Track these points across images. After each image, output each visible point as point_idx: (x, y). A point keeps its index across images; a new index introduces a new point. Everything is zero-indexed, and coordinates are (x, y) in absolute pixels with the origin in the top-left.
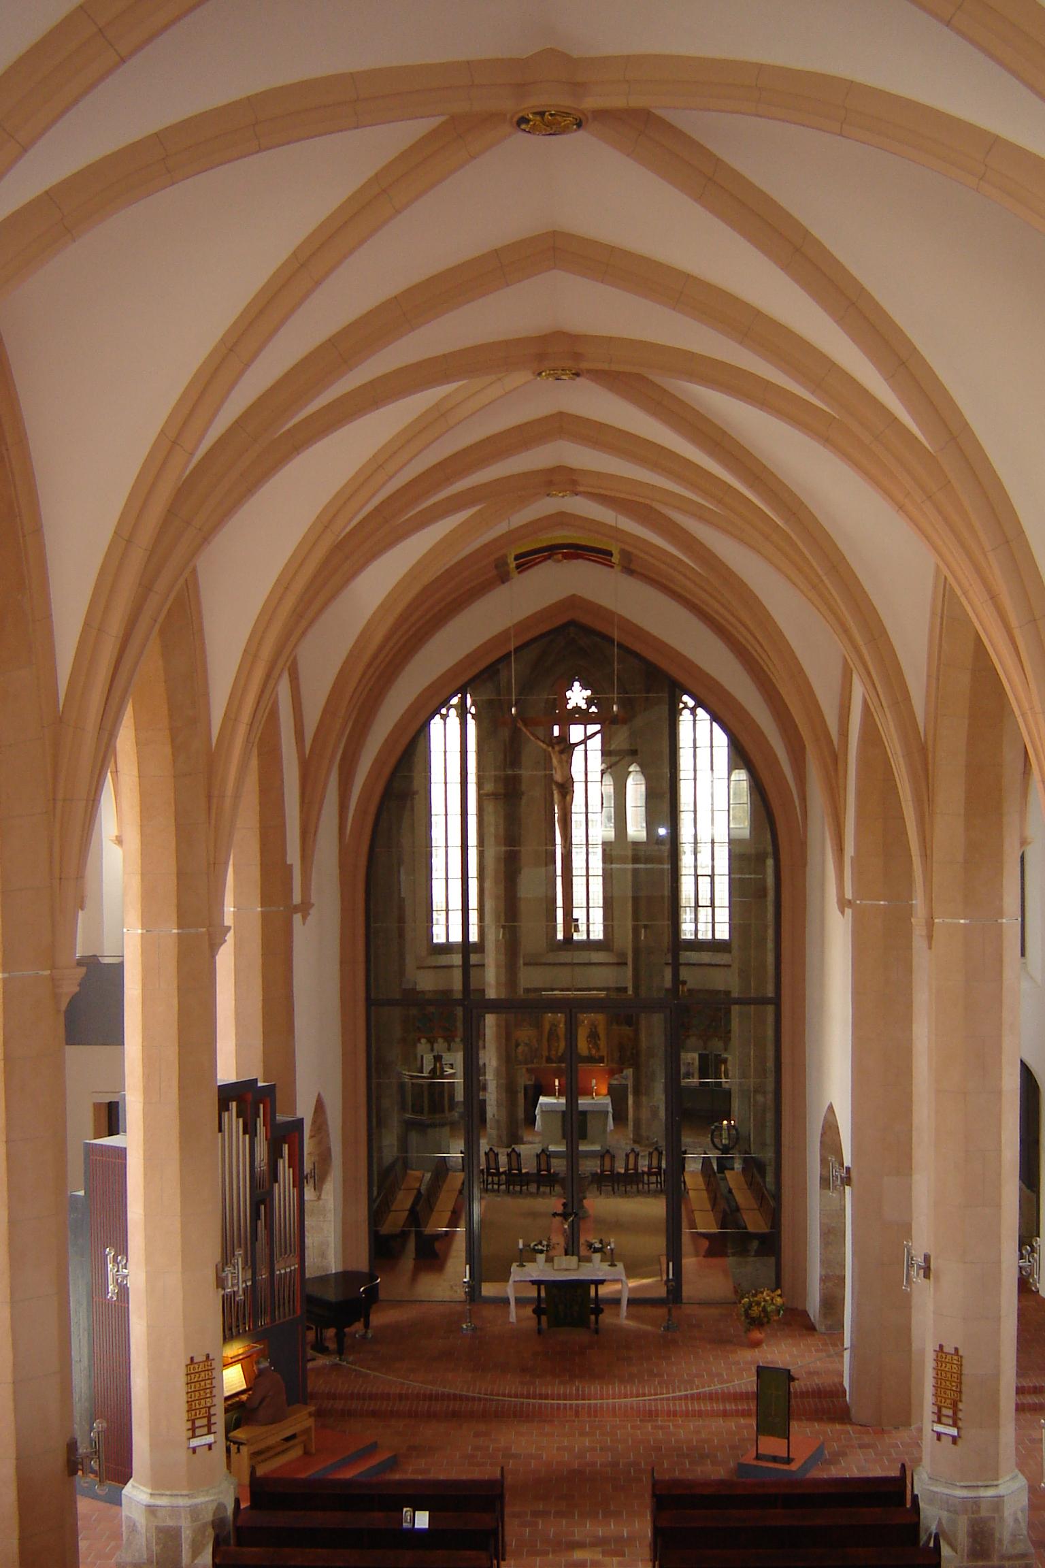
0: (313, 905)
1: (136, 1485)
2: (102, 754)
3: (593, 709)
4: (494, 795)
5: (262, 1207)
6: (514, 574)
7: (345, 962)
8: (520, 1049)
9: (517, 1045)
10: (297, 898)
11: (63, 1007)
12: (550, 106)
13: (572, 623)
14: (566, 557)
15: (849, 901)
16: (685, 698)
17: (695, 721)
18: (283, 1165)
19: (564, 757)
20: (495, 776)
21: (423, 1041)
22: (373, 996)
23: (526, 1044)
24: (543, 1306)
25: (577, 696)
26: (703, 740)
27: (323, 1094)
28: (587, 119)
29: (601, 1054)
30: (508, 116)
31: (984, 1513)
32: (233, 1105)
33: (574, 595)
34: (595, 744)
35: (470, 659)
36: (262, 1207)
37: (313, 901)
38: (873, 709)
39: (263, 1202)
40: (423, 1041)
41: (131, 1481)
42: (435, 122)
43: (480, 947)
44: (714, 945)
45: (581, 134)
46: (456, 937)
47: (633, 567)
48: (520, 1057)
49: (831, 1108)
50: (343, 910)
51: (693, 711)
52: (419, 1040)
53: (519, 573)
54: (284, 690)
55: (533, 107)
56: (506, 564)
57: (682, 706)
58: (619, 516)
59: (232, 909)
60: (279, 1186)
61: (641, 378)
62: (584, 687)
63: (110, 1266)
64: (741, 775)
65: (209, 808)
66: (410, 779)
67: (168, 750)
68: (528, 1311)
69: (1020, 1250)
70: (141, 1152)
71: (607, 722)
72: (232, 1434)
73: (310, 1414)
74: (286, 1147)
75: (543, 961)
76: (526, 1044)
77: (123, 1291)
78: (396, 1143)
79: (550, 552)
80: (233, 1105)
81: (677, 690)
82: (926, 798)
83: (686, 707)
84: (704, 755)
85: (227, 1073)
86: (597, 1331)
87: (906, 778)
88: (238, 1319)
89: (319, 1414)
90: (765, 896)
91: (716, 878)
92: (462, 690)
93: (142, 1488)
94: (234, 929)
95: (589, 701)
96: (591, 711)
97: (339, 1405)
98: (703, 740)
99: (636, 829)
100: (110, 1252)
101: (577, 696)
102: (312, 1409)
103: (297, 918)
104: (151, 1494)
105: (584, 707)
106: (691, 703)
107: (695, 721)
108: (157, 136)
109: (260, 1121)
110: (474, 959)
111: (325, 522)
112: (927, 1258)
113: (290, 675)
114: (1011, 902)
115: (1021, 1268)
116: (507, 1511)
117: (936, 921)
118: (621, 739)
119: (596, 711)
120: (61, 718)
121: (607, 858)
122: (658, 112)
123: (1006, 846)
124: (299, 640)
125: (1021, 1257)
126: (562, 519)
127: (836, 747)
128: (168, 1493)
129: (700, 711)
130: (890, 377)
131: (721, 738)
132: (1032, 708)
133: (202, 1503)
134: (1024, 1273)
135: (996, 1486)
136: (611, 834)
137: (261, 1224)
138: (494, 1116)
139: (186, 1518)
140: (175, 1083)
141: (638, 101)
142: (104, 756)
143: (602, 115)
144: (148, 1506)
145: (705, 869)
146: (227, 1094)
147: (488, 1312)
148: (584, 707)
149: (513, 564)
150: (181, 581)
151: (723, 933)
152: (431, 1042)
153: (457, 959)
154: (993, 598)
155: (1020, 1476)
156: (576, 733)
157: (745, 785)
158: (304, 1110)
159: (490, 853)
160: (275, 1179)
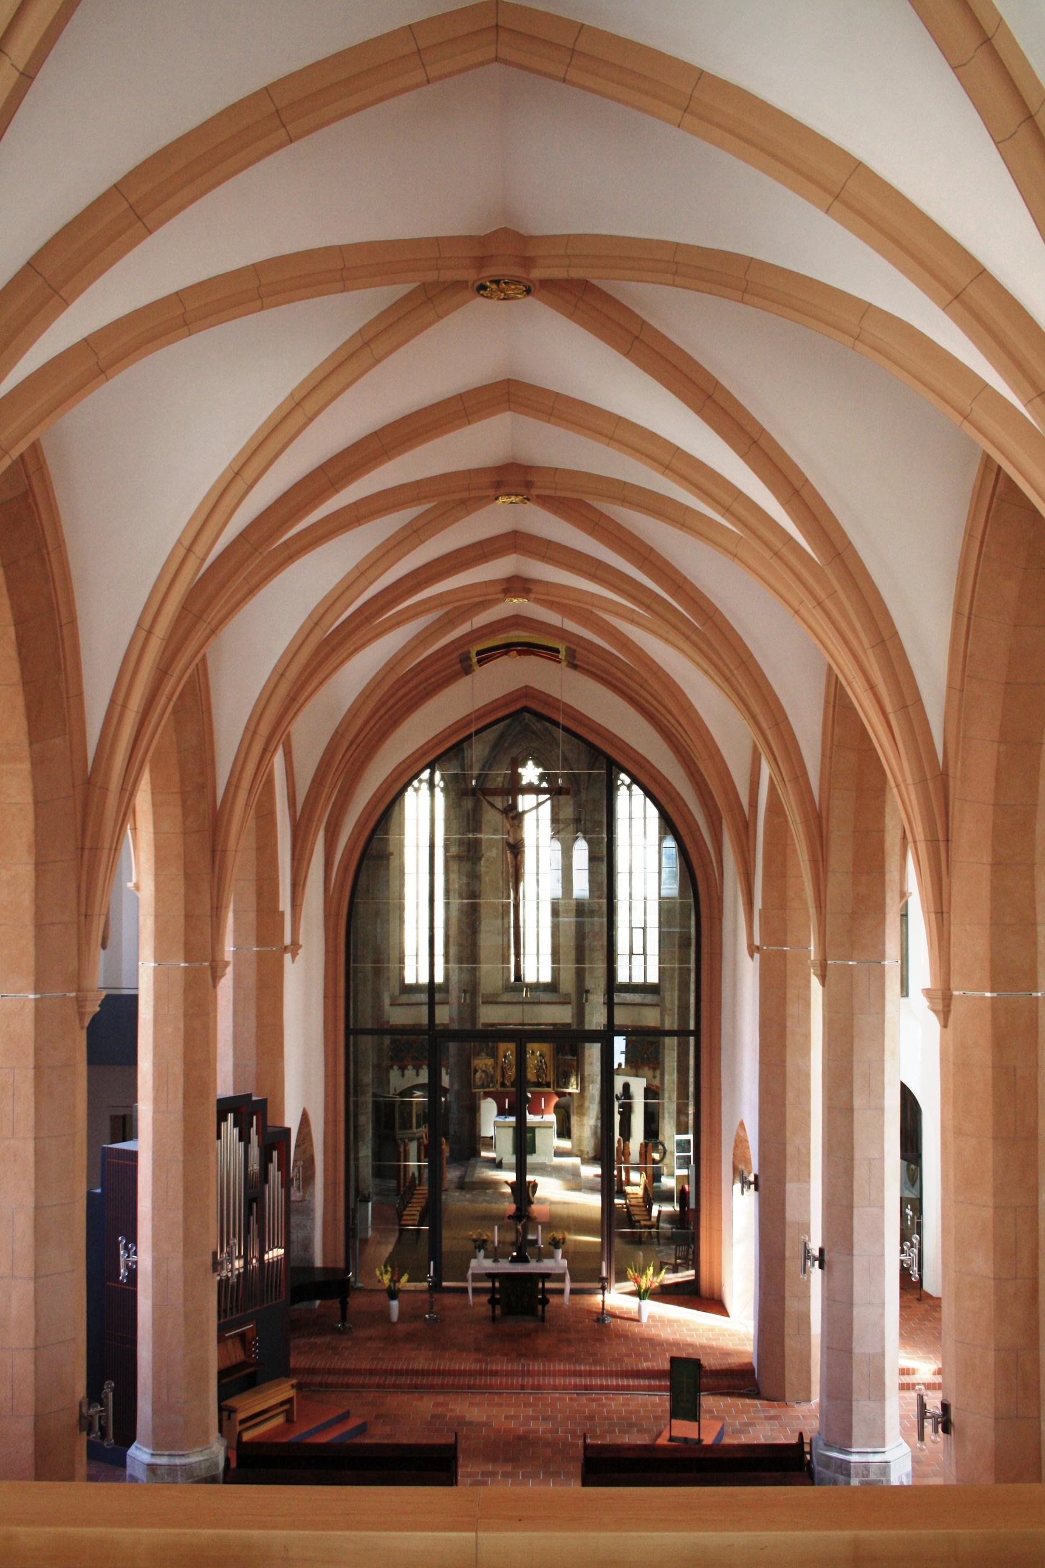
0: (301, 946)
1: (139, 1446)
2: (123, 810)
3: (544, 785)
4: (459, 858)
5: (255, 1205)
6: (476, 667)
7: (328, 996)
8: (478, 1075)
9: (476, 1071)
10: (287, 940)
11: (87, 1024)
12: (504, 275)
13: (525, 709)
14: (520, 653)
15: (758, 948)
16: (623, 776)
17: (631, 795)
18: (273, 1167)
19: (516, 822)
20: (460, 839)
21: (396, 1068)
22: (351, 1027)
23: (483, 1071)
24: (498, 1296)
25: (530, 773)
26: (638, 812)
27: (308, 1110)
28: (535, 288)
29: (548, 1080)
30: (470, 284)
31: (873, 1477)
32: (230, 1117)
33: (526, 686)
34: (546, 810)
35: (439, 739)
36: (255, 1205)
37: (301, 942)
38: (776, 783)
39: (255, 1200)
40: (396, 1068)
41: (135, 1443)
42: (412, 286)
43: (445, 987)
44: (644, 988)
45: (530, 299)
46: (424, 979)
47: (576, 662)
48: (479, 1083)
49: (742, 1124)
50: (327, 952)
51: (629, 787)
52: (391, 1067)
53: (480, 666)
54: (278, 761)
55: (492, 276)
56: (469, 658)
57: (619, 782)
58: (565, 619)
59: (232, 949)
60: (269, 1187)
61: (581, 503)
62: (538, 764)
63: (122, 1252)
64: (670, 843)
65: (213, 862)
66: (385, 842)
67: (179, 811)
68: (484, 1299)
69: (901, 1245)
70: (151, 1153)
71: (554, 792)
72: (224, 1403)
73: (293, 1386)
74: (275, 1154)
75: (500, 1000)
76: (483, 1071)
77: (133, 1273)
78: (370, 1154)
79: (506, 648)
80: (230, 1116)
81: (614, 767)
82: (820, 859)
83: (623, 784)
84: (638, 824)
85: (225, 1087)
86: (543, 1319)
87: (802, 836)
88: (231, 1303)
89: (299, 1387)
90: (689, 945)
91: (648, 930)
92: (432, 766)
93: (145, 1449)
94: (234, 964)
95: (542, 778)
96: (542, 786)
97: (318, 1379)
98: (638, 812)
99: (581, 887)
100: (122, 1240)
101: (530, 773)
102: (294, 1381)
103: (288, 957)
104: (152, 1455)
105: (536, 782)
106: (627, 780)
107: (631, 795)
108: (178, 296)
109: (253, 1130)
110: (438, 997)
111: (316, 620)
112: (821, 1251)
113: (284, 750)
114: (892, 948)
115: (902, 1261)
116: (460, 1471)
117: (829, 962)
118: (568, 812)
119: (546, 786)
120: (89, 779)
121: (555, 912)
122: (595, 282)
123: (888, 900)
124: (292, 719)
125: (902, 1251)
126: (517, 621)
127: (747, 816)
128: (167, 1453)
129: (635, 787)
130: (785, 504)
131: (653, 812)
132: (904, 781)
133: (196, 1463)
134: (905, 1265)
135: (883, 1452)
136: (559, 893)
137: (253, 1219)
138: (455, 1132)
139: (182, 1476)
140: (180, 1095)
141: (576, 273)
142: (126, 811)
143: (547, 284)
144: (149, 1465)
145: (638, 922)
146: (224, 1107)
147: (448, 1300)
148: (536, 782)
149: (475, 660)
150: (193, 666)
151: (653, 978)
152: (403, 1069)
153: (424, 997)
154: (872, 688)
155: (905, 1445)
156: (525, 802)
157: (674, 852)
158: (291, 1121)
159: (455, 902)
160: (266, 1180)
